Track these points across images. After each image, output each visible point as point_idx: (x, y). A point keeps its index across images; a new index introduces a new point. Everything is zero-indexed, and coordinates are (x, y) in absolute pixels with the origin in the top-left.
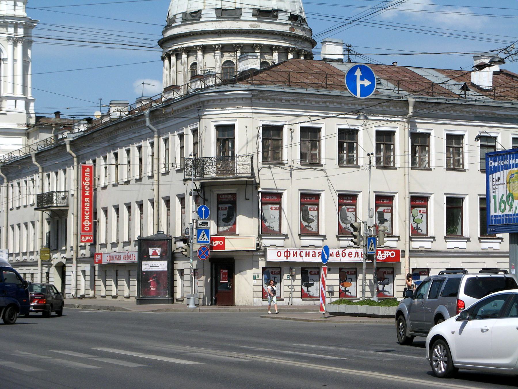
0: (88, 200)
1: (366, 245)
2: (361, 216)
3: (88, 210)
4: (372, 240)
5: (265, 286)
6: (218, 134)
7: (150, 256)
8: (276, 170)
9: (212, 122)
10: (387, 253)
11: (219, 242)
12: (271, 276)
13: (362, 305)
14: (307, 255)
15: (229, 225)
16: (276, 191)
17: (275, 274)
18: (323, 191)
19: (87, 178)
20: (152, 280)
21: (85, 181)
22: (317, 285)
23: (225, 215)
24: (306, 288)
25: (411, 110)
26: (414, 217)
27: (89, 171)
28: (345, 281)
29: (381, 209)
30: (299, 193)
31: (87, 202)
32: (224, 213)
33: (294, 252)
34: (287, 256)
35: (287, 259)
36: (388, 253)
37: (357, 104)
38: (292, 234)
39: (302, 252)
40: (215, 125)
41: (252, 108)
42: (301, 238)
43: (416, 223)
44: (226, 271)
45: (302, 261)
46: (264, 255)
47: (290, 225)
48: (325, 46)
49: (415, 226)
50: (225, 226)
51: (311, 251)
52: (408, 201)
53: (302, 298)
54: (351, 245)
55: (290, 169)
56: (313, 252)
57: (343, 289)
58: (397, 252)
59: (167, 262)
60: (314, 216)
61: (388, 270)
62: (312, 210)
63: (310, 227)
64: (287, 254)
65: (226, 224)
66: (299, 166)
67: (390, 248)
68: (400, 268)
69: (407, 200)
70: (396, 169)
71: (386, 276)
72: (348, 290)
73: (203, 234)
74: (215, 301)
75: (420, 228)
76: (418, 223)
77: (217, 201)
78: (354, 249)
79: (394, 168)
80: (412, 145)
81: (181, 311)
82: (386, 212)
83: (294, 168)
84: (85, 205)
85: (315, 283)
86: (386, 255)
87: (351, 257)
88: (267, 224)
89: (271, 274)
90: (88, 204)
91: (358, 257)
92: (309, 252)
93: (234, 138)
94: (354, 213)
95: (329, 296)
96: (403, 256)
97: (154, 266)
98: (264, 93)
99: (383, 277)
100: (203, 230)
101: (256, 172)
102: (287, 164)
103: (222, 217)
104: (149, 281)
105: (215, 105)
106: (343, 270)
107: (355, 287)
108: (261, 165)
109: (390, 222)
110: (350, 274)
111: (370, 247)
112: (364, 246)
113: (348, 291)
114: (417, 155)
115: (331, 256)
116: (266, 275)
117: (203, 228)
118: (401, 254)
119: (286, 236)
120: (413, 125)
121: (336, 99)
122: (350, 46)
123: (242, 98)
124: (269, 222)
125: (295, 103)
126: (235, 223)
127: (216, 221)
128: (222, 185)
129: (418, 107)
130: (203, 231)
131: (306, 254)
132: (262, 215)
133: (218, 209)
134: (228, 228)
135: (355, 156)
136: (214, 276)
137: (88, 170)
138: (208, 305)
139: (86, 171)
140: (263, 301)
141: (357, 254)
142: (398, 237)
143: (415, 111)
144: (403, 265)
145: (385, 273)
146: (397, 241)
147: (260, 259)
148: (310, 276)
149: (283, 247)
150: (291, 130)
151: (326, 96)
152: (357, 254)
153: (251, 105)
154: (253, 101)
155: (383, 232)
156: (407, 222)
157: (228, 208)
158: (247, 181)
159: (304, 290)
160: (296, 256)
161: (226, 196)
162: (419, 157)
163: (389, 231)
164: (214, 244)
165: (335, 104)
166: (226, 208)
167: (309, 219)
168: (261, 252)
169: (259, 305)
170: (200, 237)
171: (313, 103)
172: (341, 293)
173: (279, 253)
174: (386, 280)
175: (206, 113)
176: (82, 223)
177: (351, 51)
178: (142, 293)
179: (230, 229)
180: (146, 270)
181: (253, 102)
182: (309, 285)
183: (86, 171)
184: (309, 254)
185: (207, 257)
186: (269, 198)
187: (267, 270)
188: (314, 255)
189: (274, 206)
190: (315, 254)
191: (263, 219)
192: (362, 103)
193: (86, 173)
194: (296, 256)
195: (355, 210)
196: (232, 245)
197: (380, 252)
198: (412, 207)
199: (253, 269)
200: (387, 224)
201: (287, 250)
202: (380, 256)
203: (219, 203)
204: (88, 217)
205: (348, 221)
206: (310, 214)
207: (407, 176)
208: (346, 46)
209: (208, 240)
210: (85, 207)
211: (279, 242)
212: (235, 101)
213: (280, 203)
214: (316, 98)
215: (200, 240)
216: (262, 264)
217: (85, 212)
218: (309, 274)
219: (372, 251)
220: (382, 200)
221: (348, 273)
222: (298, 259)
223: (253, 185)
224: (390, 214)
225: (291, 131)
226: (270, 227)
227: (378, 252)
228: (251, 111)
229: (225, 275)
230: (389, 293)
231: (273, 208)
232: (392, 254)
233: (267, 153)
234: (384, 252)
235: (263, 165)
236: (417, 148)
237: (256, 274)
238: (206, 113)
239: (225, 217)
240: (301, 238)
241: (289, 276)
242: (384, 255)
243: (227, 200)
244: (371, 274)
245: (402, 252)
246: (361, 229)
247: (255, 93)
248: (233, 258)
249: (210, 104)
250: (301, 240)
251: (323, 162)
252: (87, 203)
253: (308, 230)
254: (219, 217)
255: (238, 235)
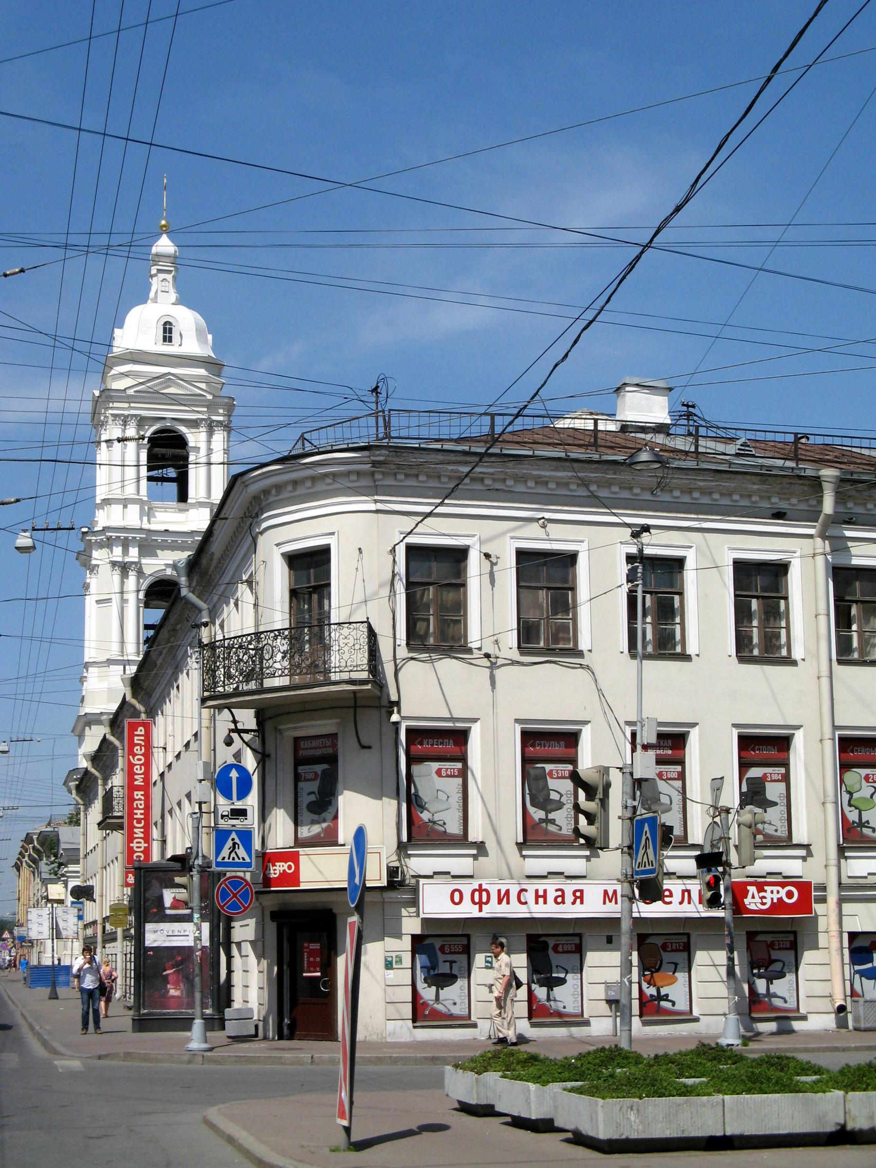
0: (142, 795)
1: (630, 847)
2: (699, 791)
3: (142, 817)
4: (646, 828)
5: (421, 985)
6: (293, 578)
7: (166, 908)
8: (448, 666)
9: (277, 545)
10: (775, 892)
11: (286, 866)
12: (441, 957)
13: (545, 1083)
14: (541, 900)
15: (324, 821)
16: (450, 724)
17: (451, 953)
18: (586, 723)
19: (138, 747)
20: (172, 971)
21: (134, 755)
22: (575, 982)
23: (313, 793)
24: (545, 989)
25: (828, 505)
26: (851, 794)
27: (143, 733)
28: (658, 971)
29: (755, 772)
30: (518, 728)
31: (140, 799)
32: (310, 787)
33: (499, 891)
34: (481, 904)
35: (481, 910)
36: (778, 892)
37: (676, 488)
38: (499, 843)
39: (526, 890)
40: (283, 555)
41: (376, 497)
42: (524, 853)
43: (856, 808)
44: (315, 946)
45: (528, 916)
46: (414, 903)
47: (493, 818)
48: (624, 395)
49: (853, 816)
50: (313, 822)
51: (551, 887)
52: (829, 753)
53: (530, 1017)
54: (671, 871)
55: (489, 664)
56: (557, 890)
57: (651, 991)
58: (804, 888)
59: (208, 923)
60: (563, 793)
61: (781, 937)
62: (558, 778)
63: (553, 822)
64: (480, 897)
65: (315, 817)
66: (516, 655)
67: (785, 877)
68: (816, 933)
69: (828, 744)
70: (794, 663)
71: (775, 955)
72: (667, 995)
73: (234, 844)
74: (292, 1027)
75: (868, 822)
76: (862, 808)
77: (295, 758)
78: (680, 881)
79: (788, 661)
80: (838, 599)
81: (158, 1061)
82: (772, 781)
83: (500, 662)
84: (135, 806)
85: (569, 977)
86: (772, 896)
87: (670, 903)
88: (425, 816)
89: (439, 953)
90: (141, 804)
91: (689, 903)
92: (545, 891)
93: (328, 585)
94: (678, 784)
95: (610, 1014)
96: (823, 900)
97: (176, 934)
98: (405, 455)
99: (766, 957)
100: (230, 832)
101: (389, 669)
102: (480, 649)
103: (306, 800)
104: (165, 973)
105: (283, 499)
106: (649, 940)
107: (687, 986)
108: (403, 652)
109: (782, 808)
110: (672, 951)
111: (641, 852)
112: (626, 849)
113: (666, 998)
114: (854, 627)
115: (610, 901)
116: (424, 957)
117: (233, 826)
118: (813, 894)
119: (481, 848)
120: (839, 545)
121: (615, 473)
122: (693, 406)
123: (348, 473)
124: (431, 810)
125: (498, 486)
126: (336, 817)
127: (291, 808)
128: (302, 712)
129: (850, 497)
130: (234, 835)
131: (537, 896)
132: (413, 791)
133: (297, 778)
134: (320, 829)
135: (678, 628)
136: (286, 959)
137: (141, 731)
138: (273, 1039)
139: (136, 733)
140: (415, 1027)
141: (686, 894)
142: (807, 847)
143: (841, 509)
144: (822, 924)
145: (771, 946)
146: (804, 859)
147: (404, 912)
148: (555, 959)
149: (471, 877)
150: (487, 556)
151: (586, 465)
152: (686, 894)
153: (374, 490)
154: (380, 480)
155: (750, 827)
156: (830, 808)
157: (320, 774)
158: (355, 692)
159: (536, 998)
160: (508, 903)
161: (315, 743)
162: (860, 633)
163: (779, 831)
164: (272, 871)
165: (615, 489)
166: (316, 773)
167: (548, 800)
168: (405, 892)
169: (403, 1040)
170: (225, 852)
171: (552, 485)
172: (647, 1004)
173: (457, 895)
174: (777, 967)
175: (264, 525)
176: (149, 845)
177: (695, 418)
178: (146, 1004)
179: (326, 831)
180: (155, 945)
181: (377, 483)
182: (551, 983)
183: (136, 733)
184: (545, 896)
185: (222, 907)
186: (432, 745)
187: (428, 941)
188: (559, 900)
189: (447, 765)
190: (563, 896)
191: (414, 802)
192: (692, 486)
193: (136, 738)
194: (508, 903)
195: (682, 776)
196: (320, 872)
197: (752, 889)
198: (845, 766)
199: (383, 940)
200: (774, 815)
201: (480, 885)
202: (753, 900)
203: (299, 762)
204: (136, 833)
205: (662, 804)
206: (550, 788)
207: (825, 681)
208: (683, 405)
209: (248, 860)
210: (135, 811)
211: (461, 864)
212: (328, 484)
213: (463, 759)
214: (556, 469)
215: (224, 858)
216: (411, 926)
217: (135, 821)
218: (551, 952)
219: (647, 867)
220: (757, 747)
221: (664, 947)
222: (513, 910)
223: (379, 707)
224: (783, 785)
225: (491, 561)
226: (434, 823)
227: (749, 888)
228: (372, 507)
229: (315, 958)
230: (786, 1002)
231: (443, 773)
232: (790, 895)
233: (425, 624)
234: (766, 888)
235: (409, 652)
236: (854, 611)
237: (394, 954)
238: (264, 525)
239: (315, 799)
240: (524, 853)
241: (489, 959)
242: (764, 897)
243: (318, 752)
244: (722, 949)
245: (817, 889)
246: (611, 791)
247: (379, 455)
248: (331, 910)
249: (272, 499)
250: (524, 857)
251: (584, 644)
252: (138, 802)
253: (547, 831)
254: (300, 799)
255: (344, 845)
